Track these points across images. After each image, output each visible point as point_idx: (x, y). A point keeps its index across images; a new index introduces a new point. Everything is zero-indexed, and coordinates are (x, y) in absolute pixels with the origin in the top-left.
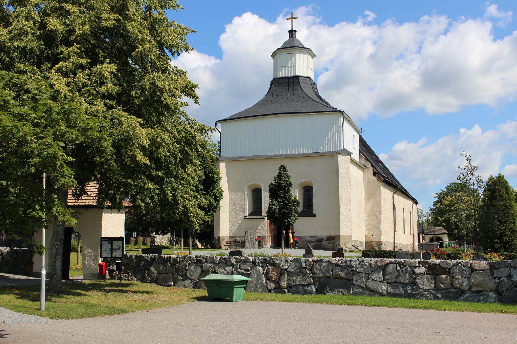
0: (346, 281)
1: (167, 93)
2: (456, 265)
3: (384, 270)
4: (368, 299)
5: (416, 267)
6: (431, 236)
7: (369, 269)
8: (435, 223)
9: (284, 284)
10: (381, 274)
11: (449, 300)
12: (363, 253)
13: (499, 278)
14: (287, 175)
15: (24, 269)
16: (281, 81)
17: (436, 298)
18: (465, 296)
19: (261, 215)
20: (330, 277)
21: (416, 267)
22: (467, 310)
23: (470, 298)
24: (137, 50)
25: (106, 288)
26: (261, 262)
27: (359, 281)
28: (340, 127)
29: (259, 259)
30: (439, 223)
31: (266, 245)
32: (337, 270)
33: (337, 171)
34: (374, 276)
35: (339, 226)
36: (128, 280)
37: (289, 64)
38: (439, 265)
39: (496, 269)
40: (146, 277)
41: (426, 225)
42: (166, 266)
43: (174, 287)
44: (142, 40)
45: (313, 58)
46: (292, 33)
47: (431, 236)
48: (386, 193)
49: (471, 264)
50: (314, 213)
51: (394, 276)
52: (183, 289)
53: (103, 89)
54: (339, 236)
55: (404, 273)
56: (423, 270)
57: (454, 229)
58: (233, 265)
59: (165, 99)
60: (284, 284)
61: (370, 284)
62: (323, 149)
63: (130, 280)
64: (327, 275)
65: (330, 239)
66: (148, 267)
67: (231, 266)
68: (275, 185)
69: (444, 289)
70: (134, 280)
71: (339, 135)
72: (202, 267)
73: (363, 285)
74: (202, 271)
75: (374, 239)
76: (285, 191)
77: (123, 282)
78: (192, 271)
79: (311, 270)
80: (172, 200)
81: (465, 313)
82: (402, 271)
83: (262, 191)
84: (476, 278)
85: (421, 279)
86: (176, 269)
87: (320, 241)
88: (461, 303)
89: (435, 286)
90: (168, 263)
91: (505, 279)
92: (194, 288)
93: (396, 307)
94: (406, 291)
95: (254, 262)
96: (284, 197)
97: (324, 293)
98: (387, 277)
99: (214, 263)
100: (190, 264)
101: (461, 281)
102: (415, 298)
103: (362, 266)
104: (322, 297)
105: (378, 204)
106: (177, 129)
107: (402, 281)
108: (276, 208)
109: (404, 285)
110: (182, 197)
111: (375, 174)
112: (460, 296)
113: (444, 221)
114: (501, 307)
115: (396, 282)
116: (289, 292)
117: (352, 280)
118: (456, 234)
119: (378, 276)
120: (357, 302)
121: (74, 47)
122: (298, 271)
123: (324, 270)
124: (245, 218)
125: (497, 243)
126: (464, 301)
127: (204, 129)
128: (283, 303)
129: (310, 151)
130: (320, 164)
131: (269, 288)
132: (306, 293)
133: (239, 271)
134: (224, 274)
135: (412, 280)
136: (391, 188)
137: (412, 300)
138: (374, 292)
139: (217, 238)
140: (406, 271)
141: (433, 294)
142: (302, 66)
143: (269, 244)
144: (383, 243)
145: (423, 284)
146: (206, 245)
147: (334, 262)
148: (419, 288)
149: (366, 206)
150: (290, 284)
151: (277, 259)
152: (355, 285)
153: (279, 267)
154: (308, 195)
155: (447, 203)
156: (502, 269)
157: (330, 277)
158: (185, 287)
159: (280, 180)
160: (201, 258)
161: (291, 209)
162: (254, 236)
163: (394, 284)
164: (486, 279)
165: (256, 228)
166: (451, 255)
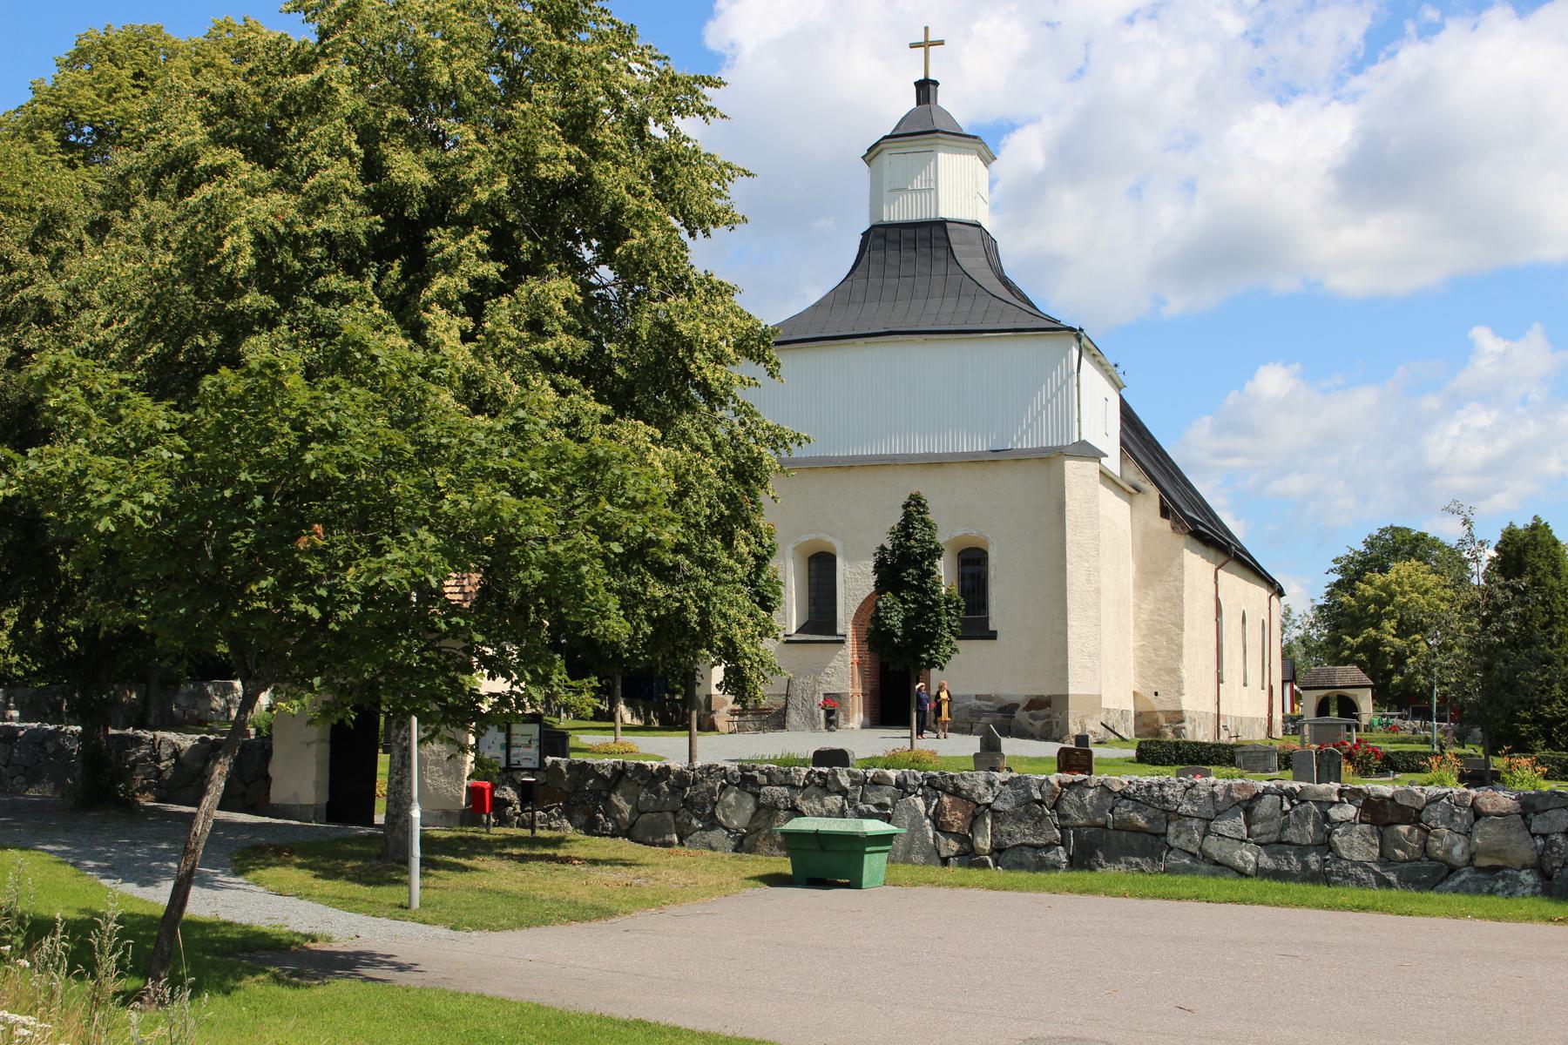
0: (1150, 838)
1: (701, 351)
2: (1435, 800)
3: (1248, 811)
4: (1211, 884)
5: (1333, 803)
6: (1323, 693)
7: (1209, 808)
8: (1333, 650)
9: (984, 842)
10: (1241, 820)
11: (1418, 890)
12: (1139, 750)
13: (1544, 836)
14: (927, 524)
15: (243, 795)
16: (892, 235)
17: (1384, 883)
18: (1458, 880)
19: (834, 632)
20: (1105, 827)
21: (1333, 803)
22: (1464, 915)
23: (1471, 885)
24: (628, 243)
25: (508, 850)
26: (921, 785)
27: (1184, 837)
28: (1070, 375)
29: (915, 778)
30: (1346, 653)
31: (847, 720)
32: (1124, 809)
34: (1224, 826)
35: (1065, 667)
36: (550, 828)
37: (917, 184)
38: (1392, 799)
39: (1536, 813)
40: (599, 820)
41: (1299, 654)
42: (657, 792)
43: (683, 850)
44: (639, 215)
45: (987, 164)
46: (925, 88)
47: (1323, 693)
48: (1197, 566)
49: (1474, 799)
51: (1275, 825)
52: (708, 853)
53: (548, 346)
55: (1302, 818)
56: (1350, 811)
57: (1390, 673)
58: (843, 792)
59: (700, 368)
60: (984, 842)
61: (1213, 846)
62: (1020, 439)
63: (556, 829)
64: (1099, 820)
65: (1038, 704)
66: (604, 794)
67: (838, 793)
68: (893, 553)
69: (1405, 861)
70: (565, 828)
71: (1066, 399)
72: (757, 796)
73: (1193, 849)
74: (759, 807)
75: (1162, 704)
76: (922, 569)
77: (539, 833)
78: (730, 806)
79: (1055, 807)
80: (699, 624)
81: (1461, 922)
82: (1296, 813)
83: (839, 562)
84: (1485, 835)
85: (1345, 833)
86: (685, 801)
87: (1009, 709)
88: (1448, 897)
89: (1381, 854)
90: (663, 784)
91: (1560, 839)
92: (735, 850)
93: (1287, 905)
94: (1306, 866)
95: (901, 785)
96: (918, 589)
97: (1092, 869)
98: (1257, 828)
99: (793, 786)
100: (723, 787)
101: (1447, 840)
102: (1328, 883)
103: (1192, 800)
104: (1087, 877)
105: (1175, 601)
106: (712, 436)
107: (1296, 840)
108: (895, 620)
109: (1302, 850)
110: (724, 616)
111: (1165, 512)
112: (1445, 878)
113: (1362, 648)
114: (1549, 907)
115: (1279, 842)
116: (996, 864)
117: (1165, 834)
118: (1396, 687)
119: (1232, 825)
120: (1184, 891)
121: (474, 237)
122: (1021, 810)
123: (1089, 809)
124: (788, 642)
125: (1525, 721)
126: (1456, 891)
127: (782, 437)
128: (991, 892)
129: (981, 445)
130: (1010, 484)
131: (944, 854)
132: (1042, 866)
133: (862, 807)
134: (821, 815)
135: (1321, 836)
136: (1212, 553)
137: (1324, 889)
138: (1221, 867)
139: (702, 699)
140: (1307, 815)
141: (1375, 873)
142: (957, 189)
143: (858, 717)
144: (1186, 715)
145: (1351, 848)
146: (647, 714)
147: (1117, 788)
148: (1341, 858)
149: (1138, 607)
150: (999, 843)
151: (963, 777)
152: (1171, 848)
153: (969, 799)
154: (973, 576)
155: (1370, 591)
156: (1554, 813)
157: (1105, 827)
158: (712, 848)
159: (909, 537)
160: (756, 773)
161: (939, 623)
162: (814, 693)
163: (1276, 846)
164: (1513, 837)
165: (818, 670)
166: (1394, 758)
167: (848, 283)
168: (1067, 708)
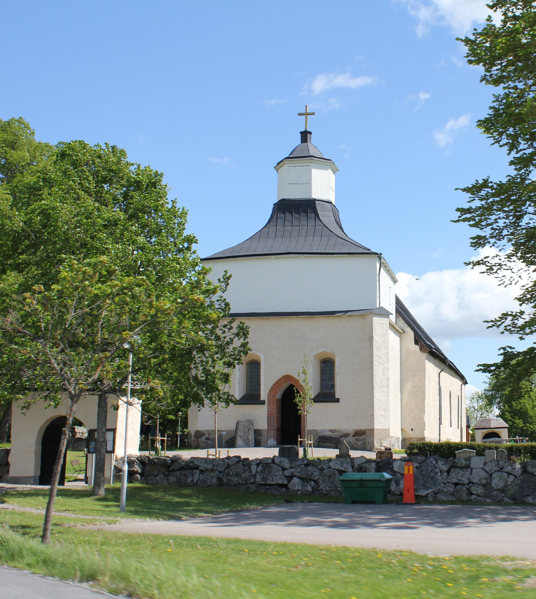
33: (371, 338)
35: (372, 415)
46: (305, 136)
48: (431, 368)
50: (337, 397)
54: (373, 430)
65: (359, 433)
111: (416, 342)
136: (437, 362)
167: (267, 228)
168: (374, 435)
